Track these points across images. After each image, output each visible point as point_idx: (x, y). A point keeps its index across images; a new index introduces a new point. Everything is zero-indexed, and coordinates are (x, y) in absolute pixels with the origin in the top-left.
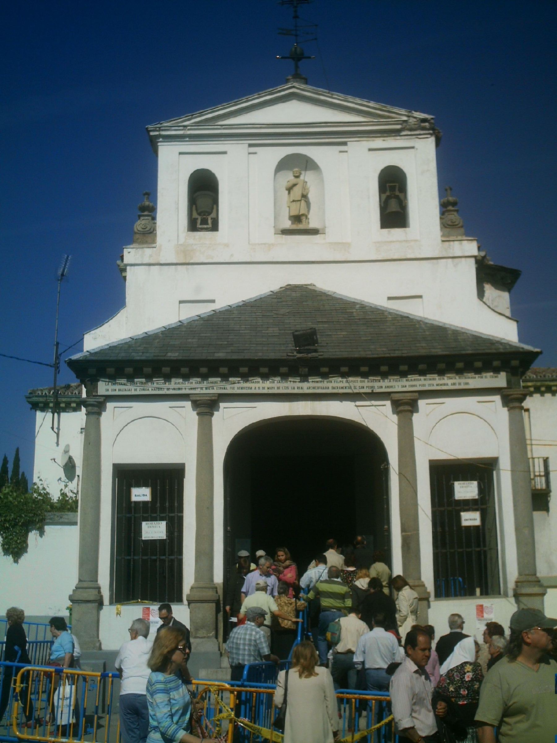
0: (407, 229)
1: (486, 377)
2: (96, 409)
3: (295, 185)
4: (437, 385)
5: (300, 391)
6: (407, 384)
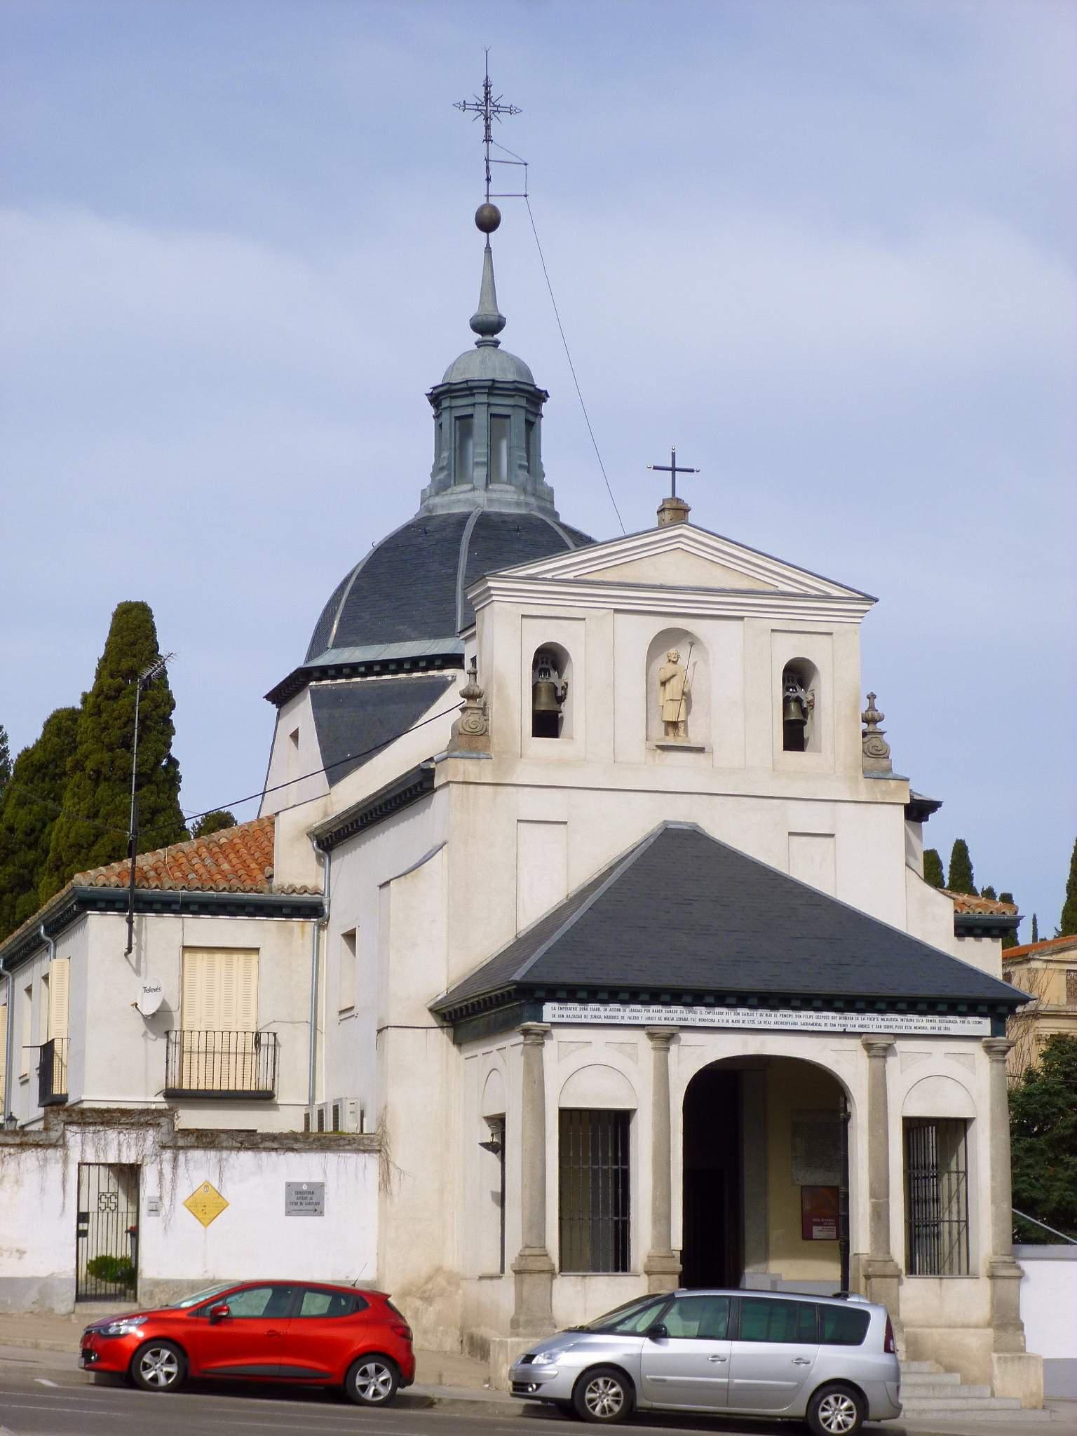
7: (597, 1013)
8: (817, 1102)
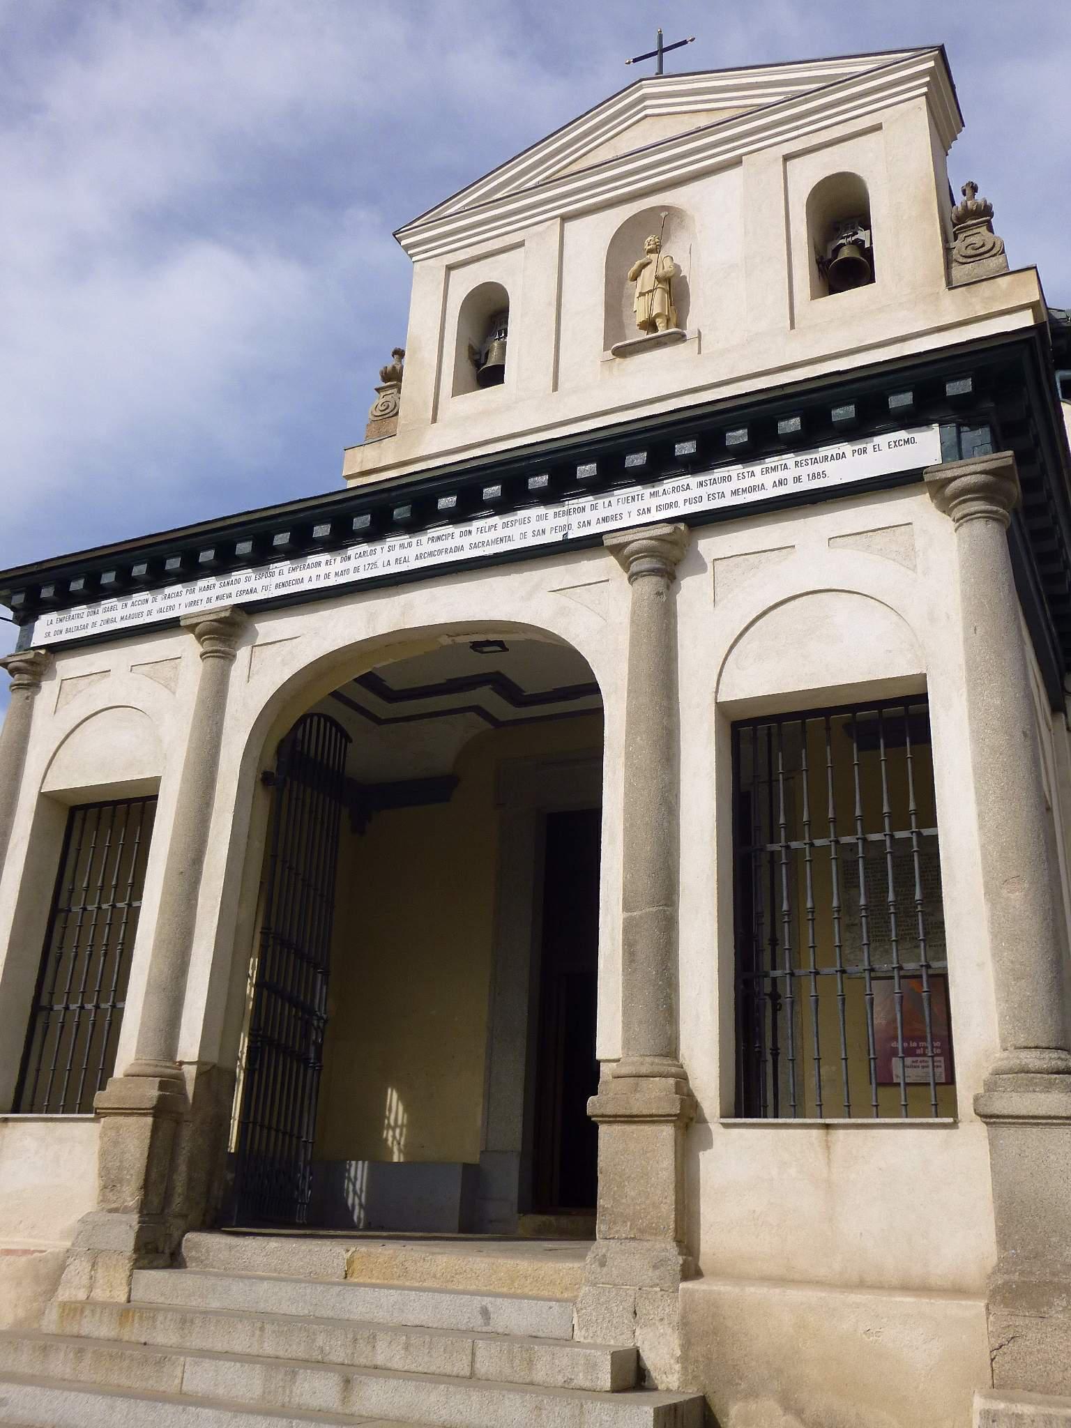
2: (25, 679)
7: (110, 615)
8: (529, 718)
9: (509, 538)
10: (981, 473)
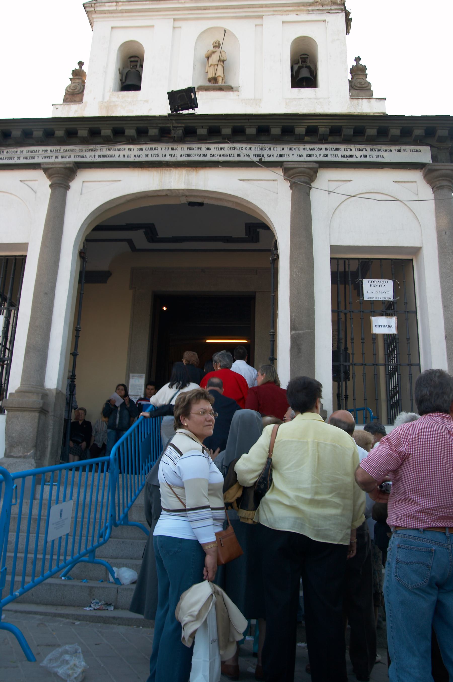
0: (317, 89)
1: (405, 151)
3: (214, 52)
4: (342, 156)
5: (173, 159)
6: (305, 153)
9: (327, 156)
10: (306, 168)
